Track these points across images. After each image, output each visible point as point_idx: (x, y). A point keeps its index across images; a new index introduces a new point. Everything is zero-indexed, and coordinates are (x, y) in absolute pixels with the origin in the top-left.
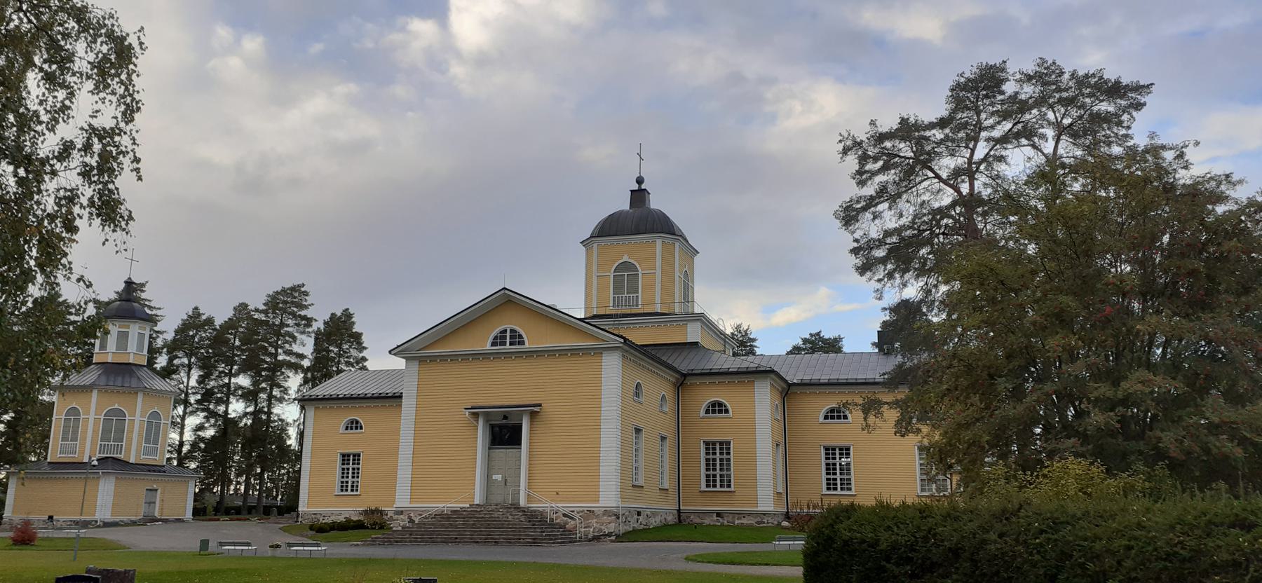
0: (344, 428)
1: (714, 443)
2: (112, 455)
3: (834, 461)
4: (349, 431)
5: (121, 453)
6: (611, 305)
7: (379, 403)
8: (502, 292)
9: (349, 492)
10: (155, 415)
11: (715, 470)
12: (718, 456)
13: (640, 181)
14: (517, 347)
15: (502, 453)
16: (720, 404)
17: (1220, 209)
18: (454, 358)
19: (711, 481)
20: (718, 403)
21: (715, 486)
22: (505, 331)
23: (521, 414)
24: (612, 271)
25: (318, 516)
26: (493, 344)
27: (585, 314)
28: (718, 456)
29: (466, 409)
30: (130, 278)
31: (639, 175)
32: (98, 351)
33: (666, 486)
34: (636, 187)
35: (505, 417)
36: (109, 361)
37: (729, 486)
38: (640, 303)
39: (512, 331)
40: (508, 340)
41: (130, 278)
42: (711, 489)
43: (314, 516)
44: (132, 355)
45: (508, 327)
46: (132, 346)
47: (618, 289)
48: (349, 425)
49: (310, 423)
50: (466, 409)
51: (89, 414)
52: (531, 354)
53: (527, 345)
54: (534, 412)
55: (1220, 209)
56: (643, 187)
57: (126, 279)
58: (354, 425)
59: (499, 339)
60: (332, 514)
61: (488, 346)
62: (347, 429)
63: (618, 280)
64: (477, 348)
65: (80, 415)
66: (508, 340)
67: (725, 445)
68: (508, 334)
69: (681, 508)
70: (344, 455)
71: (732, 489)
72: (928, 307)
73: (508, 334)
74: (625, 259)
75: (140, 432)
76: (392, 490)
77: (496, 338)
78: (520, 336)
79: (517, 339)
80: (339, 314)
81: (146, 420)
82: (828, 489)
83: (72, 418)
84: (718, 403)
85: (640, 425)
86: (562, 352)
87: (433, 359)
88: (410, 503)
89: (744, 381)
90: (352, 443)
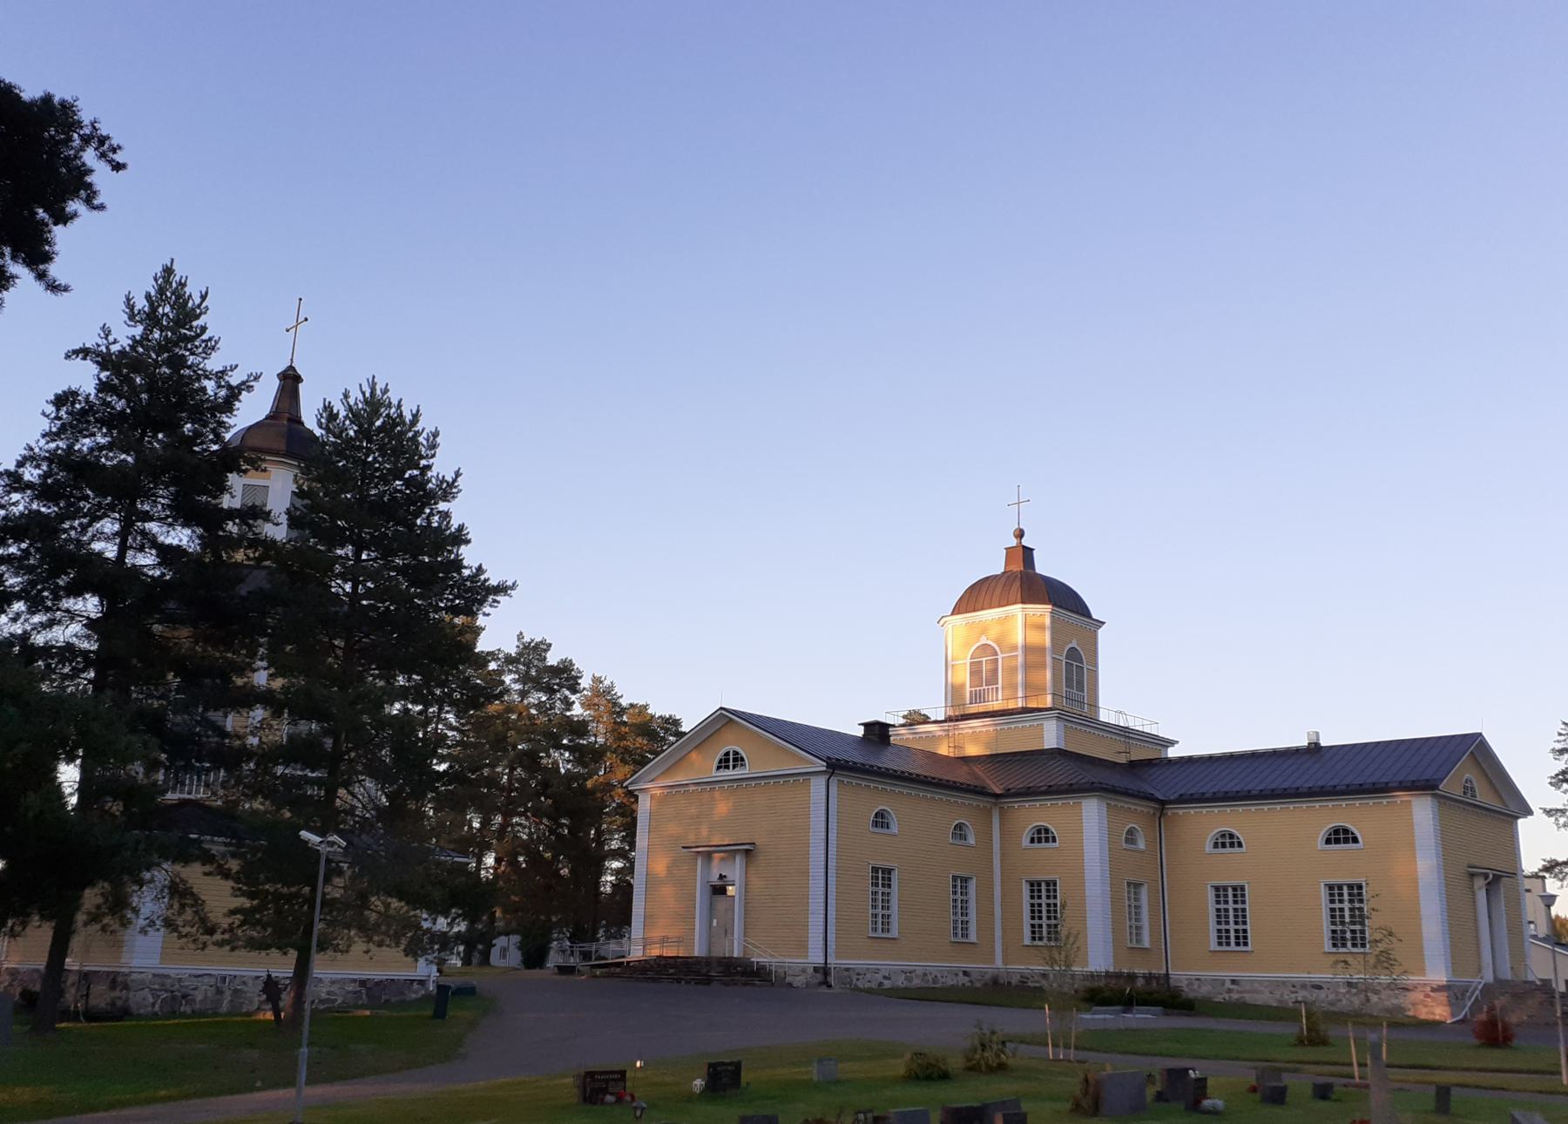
0: (1029, 840)
1: (1225, 889)
11: (1227, 923)
13: (1020, 534)
16: (1346, 831)
17: (47, 248)
19: (1223, 937)
20: (1230, 834)
21: (1228, 944)
24: (969, 658)
29: (684, 847)
33: (1528, 894)
37: (1246, 944)
42: (1224, 948)
48: (1036, 836)
50: (684, 847)
55: (47, 248)
58: (1043, 835)
59: (724, 763)
62: (1032, 841)
67: (1239, 891)
69: (1170, 972)
71: (1249, 948)
72: (80, 685)
76: (693, 950)
80: (649, 711)
84: (1230, 834)
89: (1368, 803)
90: (1343, 865)
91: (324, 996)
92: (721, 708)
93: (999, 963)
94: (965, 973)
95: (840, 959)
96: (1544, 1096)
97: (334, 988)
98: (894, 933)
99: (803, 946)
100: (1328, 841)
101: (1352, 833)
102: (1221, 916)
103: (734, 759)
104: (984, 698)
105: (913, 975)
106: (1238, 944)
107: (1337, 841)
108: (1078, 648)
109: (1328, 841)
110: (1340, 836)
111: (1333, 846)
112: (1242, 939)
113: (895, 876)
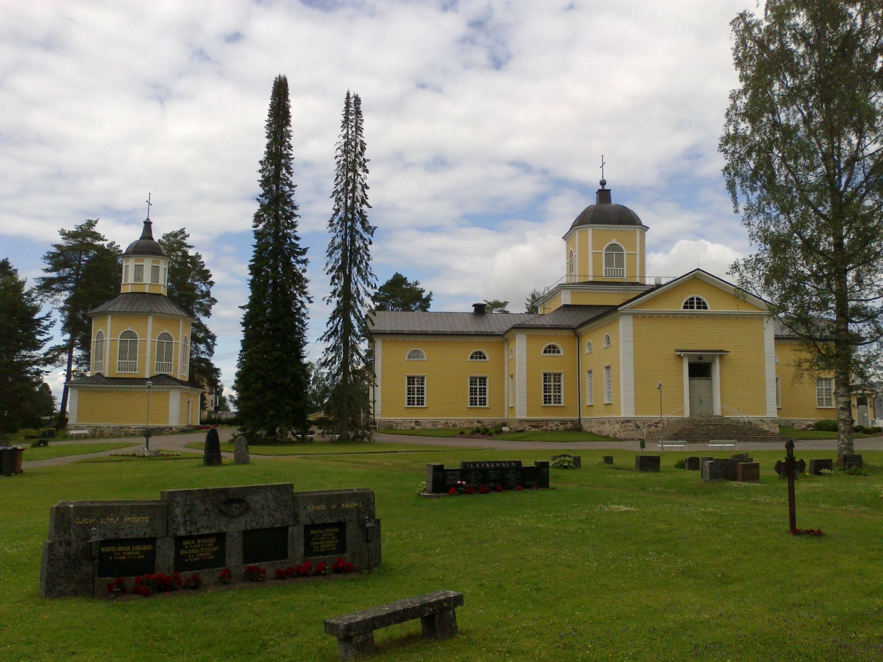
2: (165, 373)
3: (475, 396)
4: (474, 360)
5: (170, 372)
6: (604, 275)
7: (439, 339)
8: (697, 271)
9: (478, 406)
10: (166, 336)
12: (478, 386)
14: (689, 310)
15: (701, 383)
18: (660, 316)
21: (476, 404)
22: (692, 299)
23: (714, 357)
25: (392, 424)
26: (685, 307)
27: (567, 280)
28: (478, 386)
30: (148, 219)
31: (602, 179)
32: (133, 282)
34: (600, 187)
35: (701, 358)
36: (146, 292)
38: (625, 275)
39: (698, 299)
40: (695, 305)
41: (148, 219)
43: (388, 424)
44: (147, 286)
45: (695, 296)
46: (147, 278)
47: (609, 263)
49: (378, 351)
51: (146, 337)
52: (714, 316)
53: (709, 309)
54: (721, 354)
56: (606, 187)
57: (145, 219)
59: (689, 304)
60: (404, 422)
61: (682, 309)
63: (608, 257)
64: (673, 310)
65: (137, 338)
66: (695, 305)
68: (695, 301)
70: (409, 378)
73: (695, 301)
74: (614, 241)
75: (152, 352)
77: (686, 303)
78: (704, 303)
79: (701, 305)
81: (157, 340)
82: (471, 405)
83: (129, 340)
85: (607, 364)
86: (729, 316)
87: (644, 316)
88: (635, 414)
90: (478, 369)
91: (132, 432)
92: (698, 269)
93: (506, 417)
94: (479, 422)
95: (529, 416)
96: (358, 452)
97: (136, 430)
98: (562, 404)
99: (682, 412)
100: (545, 352)
101: (473, 354)
102: (558, 388)
103: (694, 304)
104: (609, 274)
105: (438, 424)
106: (480, 404)
107: (550, 352)
108: (617, 243)
109: (545, 352)
110: (479, 355)
111: (547, 354)
112: (421, 401)
113: (487, 380)
